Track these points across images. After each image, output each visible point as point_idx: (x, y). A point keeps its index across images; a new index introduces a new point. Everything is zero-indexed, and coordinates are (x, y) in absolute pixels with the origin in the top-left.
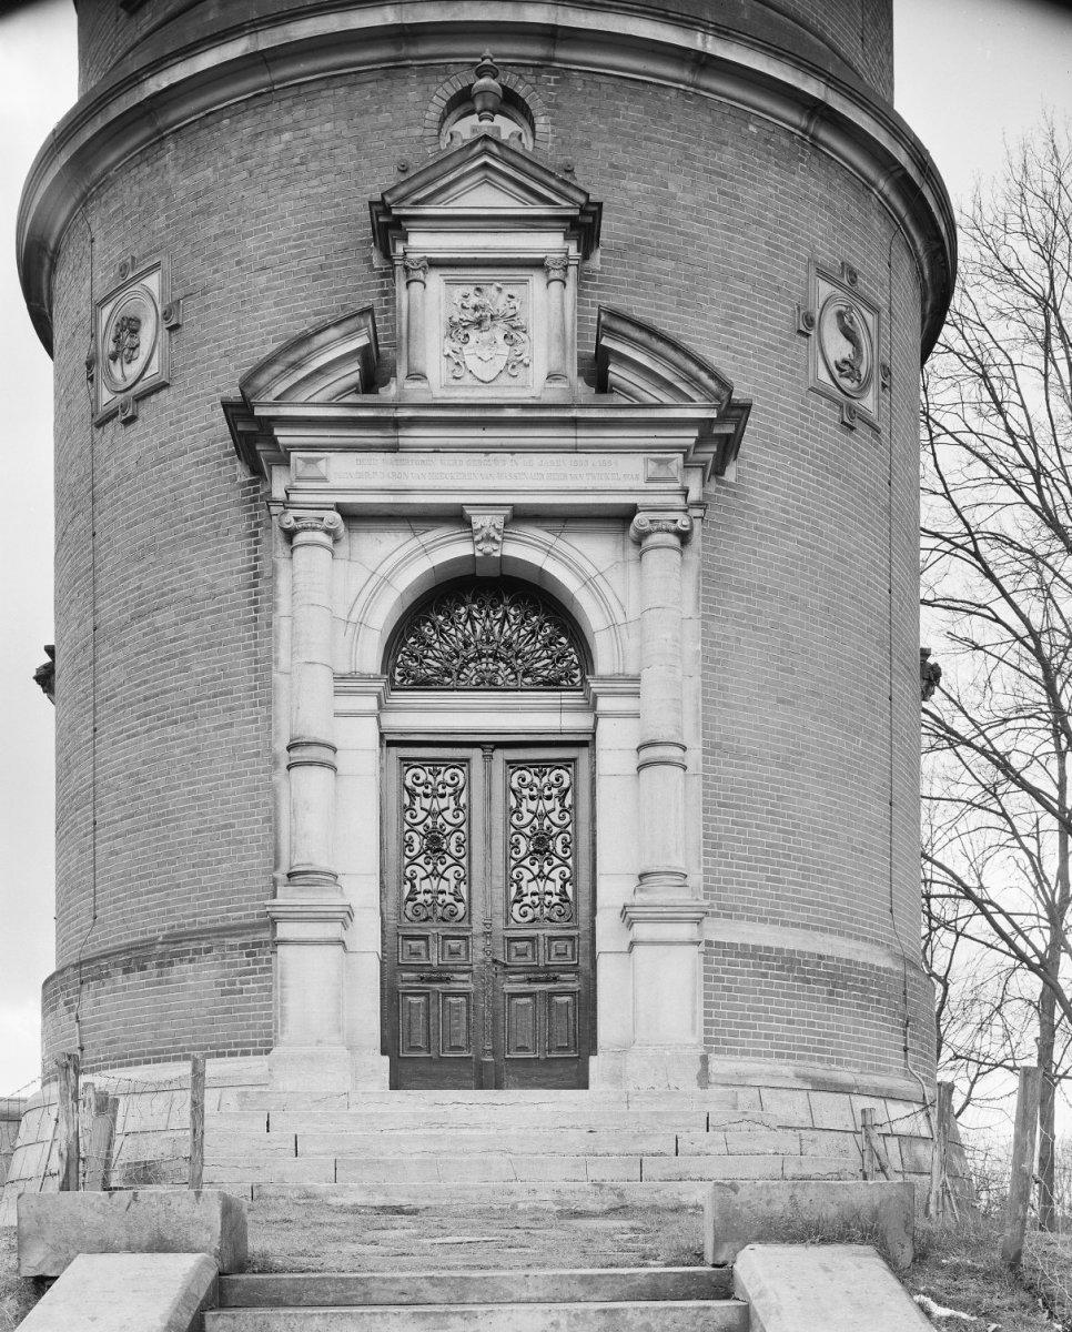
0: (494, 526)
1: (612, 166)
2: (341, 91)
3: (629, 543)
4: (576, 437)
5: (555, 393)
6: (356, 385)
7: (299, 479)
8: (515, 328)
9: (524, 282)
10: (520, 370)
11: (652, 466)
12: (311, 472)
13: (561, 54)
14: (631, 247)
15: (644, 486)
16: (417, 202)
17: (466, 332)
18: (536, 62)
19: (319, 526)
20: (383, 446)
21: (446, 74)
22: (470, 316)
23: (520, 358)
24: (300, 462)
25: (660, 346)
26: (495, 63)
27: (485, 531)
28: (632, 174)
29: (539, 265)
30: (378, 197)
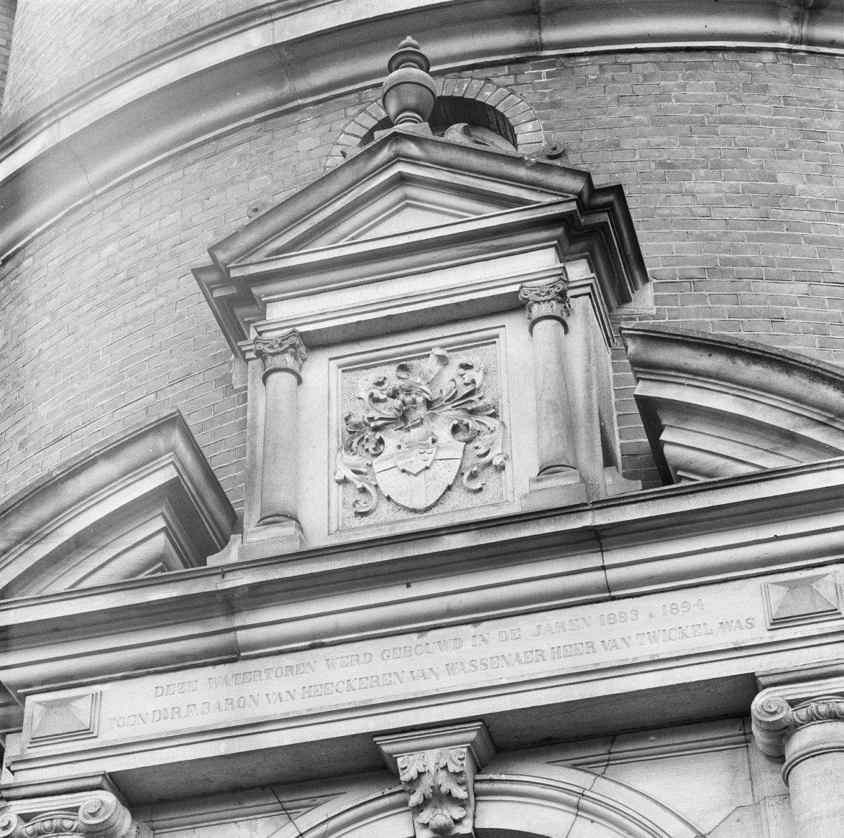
0: (445, 768)
1: (662, 164)
2: (194, 169)
3: (760, 762)
4: (604, 568)
5: (557, 491)
6: (161, 560)
7: (35, 740)
8: (472, 412)
9: (491, 340)
10: (489, 478)
11: (777, 595)
12: (59, 723)
13: (552, 35)
14: (711, 271)
15: (767, 637)
16: (279, 251)
17: (378, 435)
18: (512, 56)
19: (67, 824)
20: (208, 653)
21: (360, 103)
22: (389, 409)
23: (487, 459)
24: (40, 708)
25: (754, 372)
26: (433, 74)
27: (427, 781)
28: (702, 171)
29: (513, 305)
30: (206, 260)
